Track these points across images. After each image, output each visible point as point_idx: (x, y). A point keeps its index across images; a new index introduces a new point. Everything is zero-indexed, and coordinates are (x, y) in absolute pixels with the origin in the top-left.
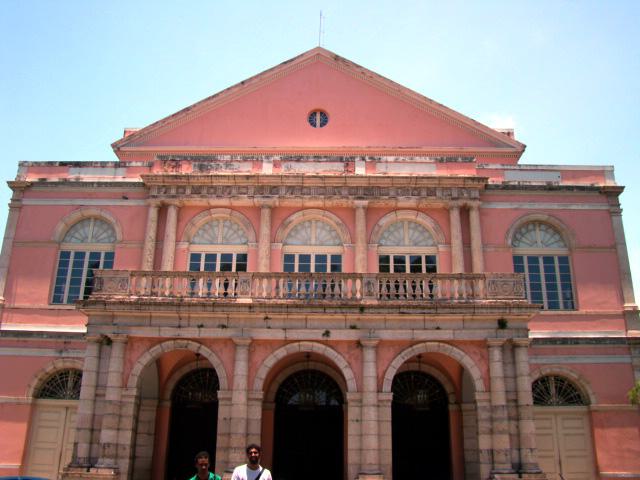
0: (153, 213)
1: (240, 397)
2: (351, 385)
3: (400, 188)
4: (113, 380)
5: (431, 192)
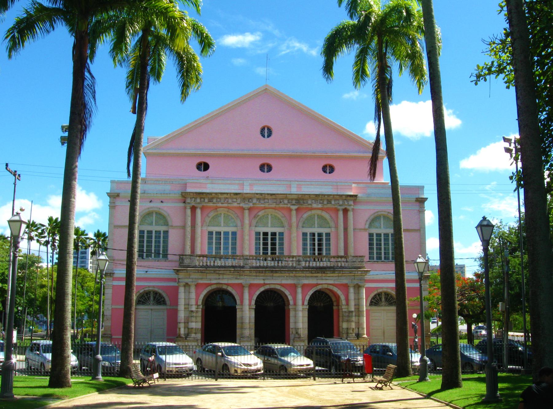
0: (189, 212)
1: (246, 307)
4: (193, 302)
5: (329, 202)
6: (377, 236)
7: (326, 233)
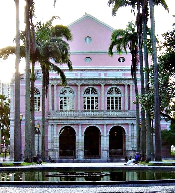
1: (80, 135)
4: (55, 133)
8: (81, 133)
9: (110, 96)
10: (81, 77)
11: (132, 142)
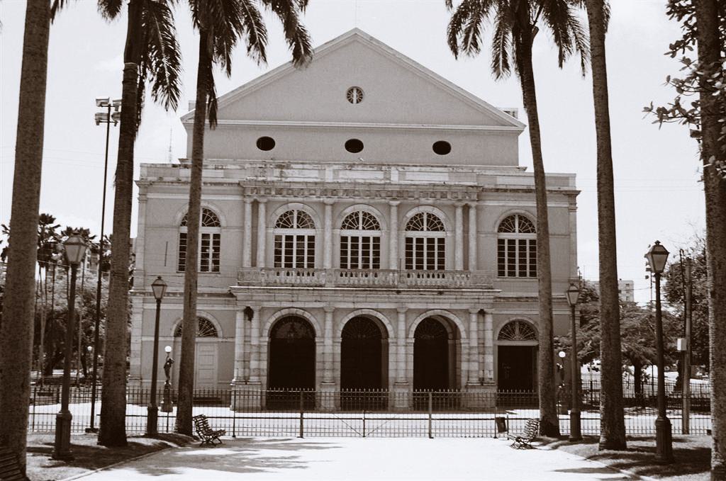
0: (248, 208)
1: (328, 342)
2: (391, 334)
3: (422, 192)
4: (255, 333)
5: (444, 196)
6: (439, 243)
7: (374, 238)
8: (330, 335)
9: (349, 233)
10: (335, 181)
11: (479, 362)
